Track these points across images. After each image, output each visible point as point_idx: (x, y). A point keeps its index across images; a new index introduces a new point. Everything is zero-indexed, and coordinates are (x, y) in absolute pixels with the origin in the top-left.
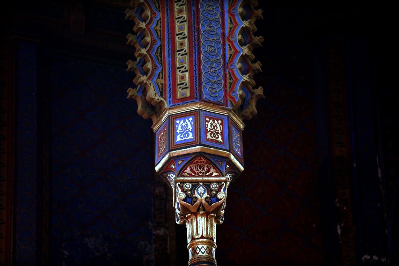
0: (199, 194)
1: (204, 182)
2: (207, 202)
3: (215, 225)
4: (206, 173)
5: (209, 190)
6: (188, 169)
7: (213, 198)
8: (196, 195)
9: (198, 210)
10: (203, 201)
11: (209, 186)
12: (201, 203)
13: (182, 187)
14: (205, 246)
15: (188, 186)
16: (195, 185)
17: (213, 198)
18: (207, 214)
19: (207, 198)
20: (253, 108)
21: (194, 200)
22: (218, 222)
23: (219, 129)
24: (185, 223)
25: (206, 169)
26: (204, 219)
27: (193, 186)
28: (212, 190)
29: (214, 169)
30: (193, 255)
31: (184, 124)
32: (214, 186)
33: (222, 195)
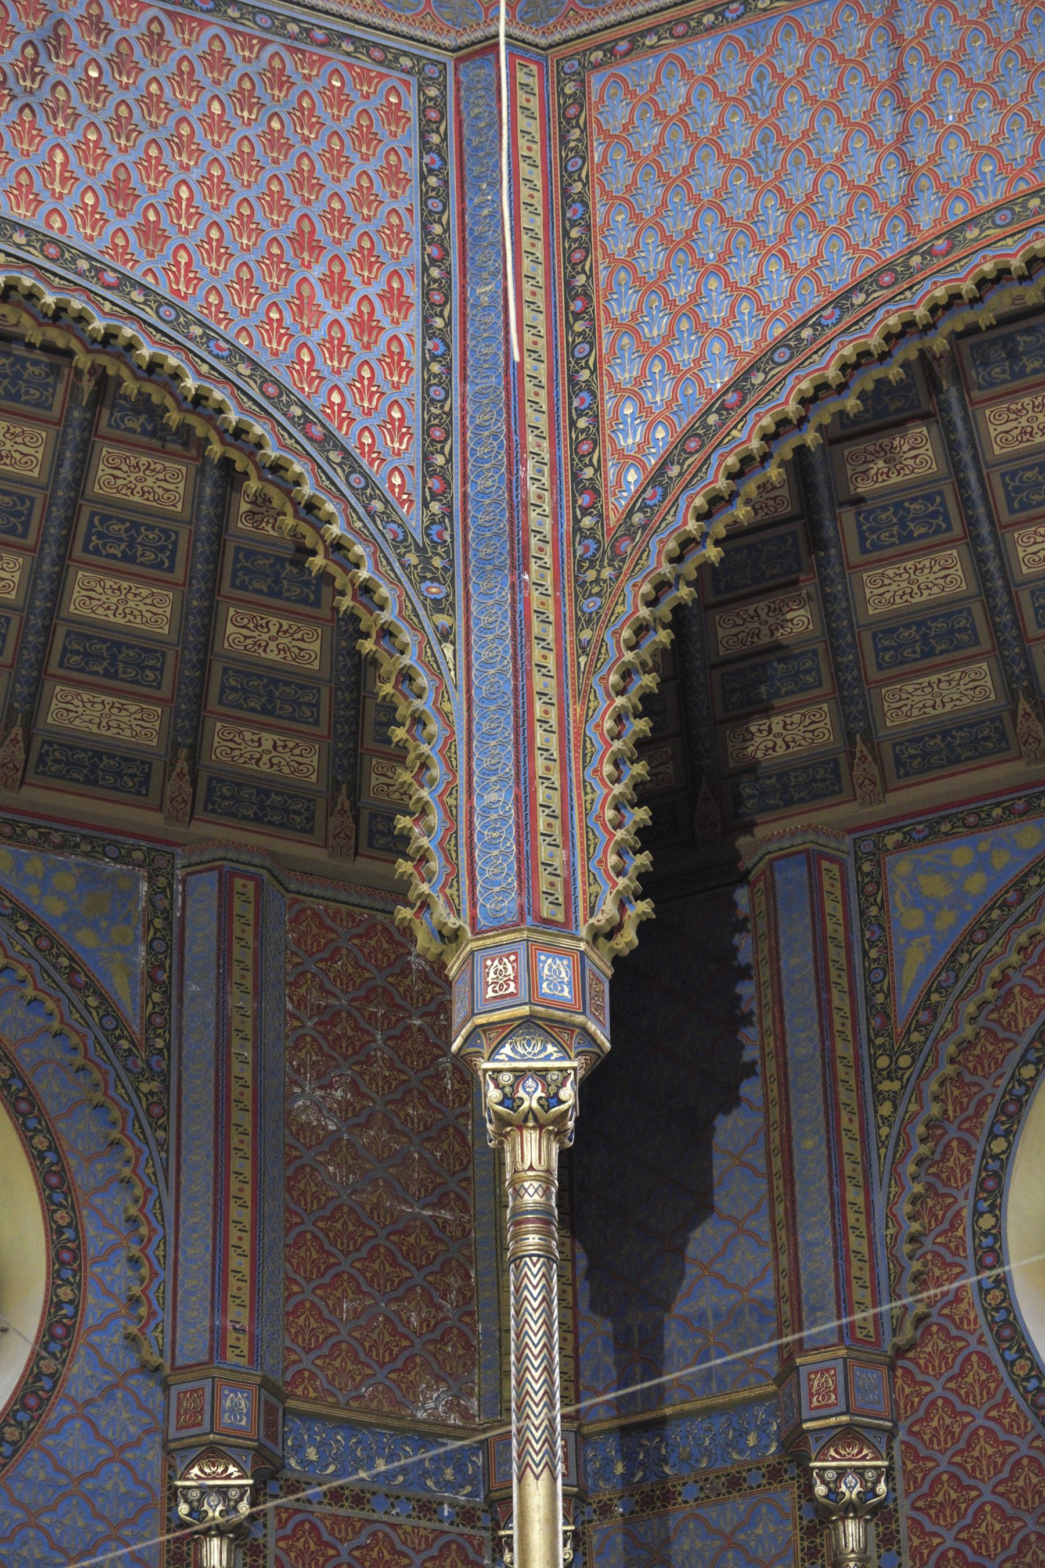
0: (528, 1093)
1: (855, 1469)
2: (542, 1106)
3: (555, 1148)
4: (540, 1052)
5: (546, 1086)
6: (508, 1046)
7: (552, 1099)
8: (843, 1489)
9: (526, 1120)
10: (535, 1105)
11: (544, 1077)
12: (531, 1109)
13: (495, 1081)
14: (536, 1184)
15: (506, 1078)
16: (841, 1473)
17: (552, 1099)
18: (540, 1126)
19: (540, 1098)
20: (629, 937)
21: (518, 1102)
22: (561, 1143)
23: (563, 975)
24: (501, 1143)
25: (538, 1048)
26: (535, 1135)
27: (517, 1078)
28: (867, 1481)
29: (554, 1045)
30: (514, 1200)
31: (501, 967)
32: (869, 1475)
33: (568, 1093)
